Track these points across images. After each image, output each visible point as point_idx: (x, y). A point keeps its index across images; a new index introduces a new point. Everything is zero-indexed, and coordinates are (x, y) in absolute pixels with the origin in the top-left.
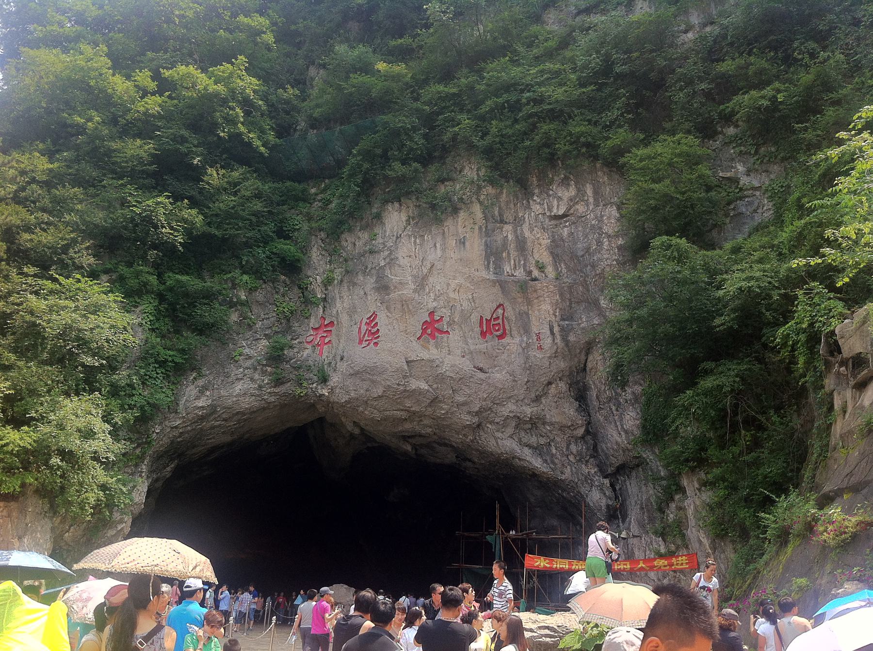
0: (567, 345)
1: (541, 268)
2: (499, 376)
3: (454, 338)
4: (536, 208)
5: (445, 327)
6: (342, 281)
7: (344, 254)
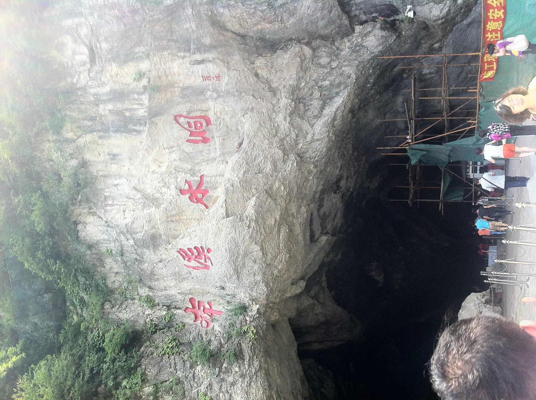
0: (215, 47)
1: (141, 75)
2: (247, 125)
3: (207, 170)
4: (83, 79)
5: (196, 178)
6: (150, 288)
7: (125, 284)
